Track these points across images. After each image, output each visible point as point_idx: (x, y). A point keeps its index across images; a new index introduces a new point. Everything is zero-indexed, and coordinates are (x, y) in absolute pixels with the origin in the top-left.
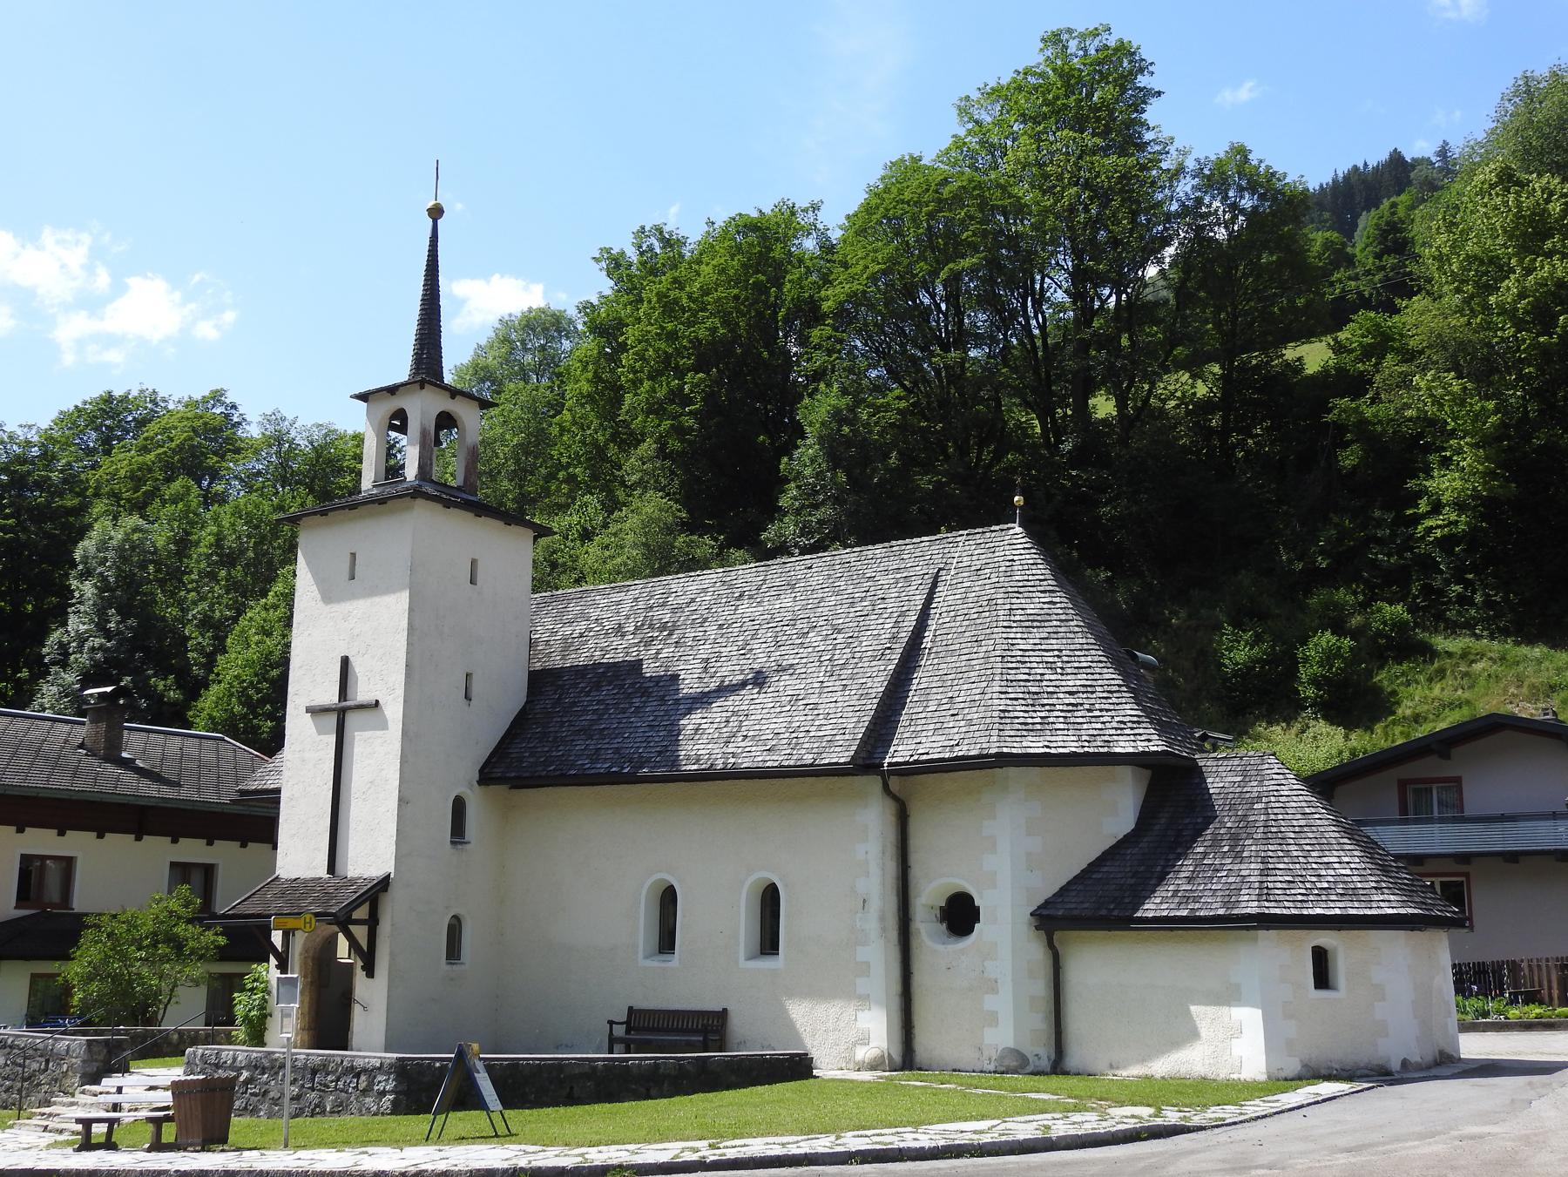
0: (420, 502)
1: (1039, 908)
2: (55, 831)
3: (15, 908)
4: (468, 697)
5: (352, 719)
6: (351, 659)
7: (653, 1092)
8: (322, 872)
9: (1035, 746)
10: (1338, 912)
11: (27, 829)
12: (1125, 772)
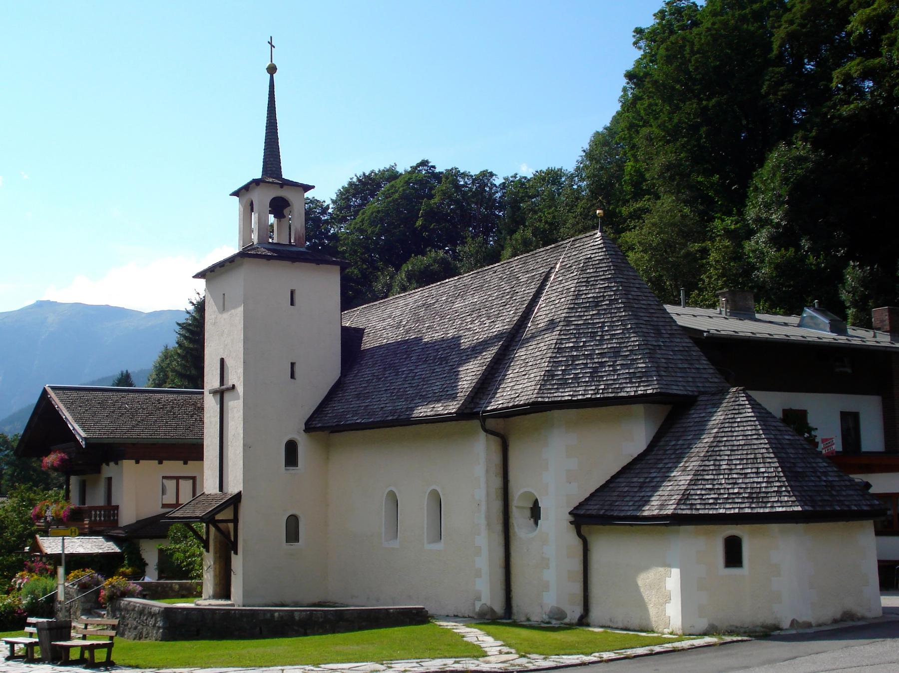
0: (247, 260)
1: (575, 508)
2: (182, 462)
3: (162, 508)
4: (293, 376)
5: (227, 396)
6: (225, 359)
7: (308, 631)
8: (217, 491)
9: (566, 395)
10: (737, 511)
11: (189, 462)
12: (639, 408)
